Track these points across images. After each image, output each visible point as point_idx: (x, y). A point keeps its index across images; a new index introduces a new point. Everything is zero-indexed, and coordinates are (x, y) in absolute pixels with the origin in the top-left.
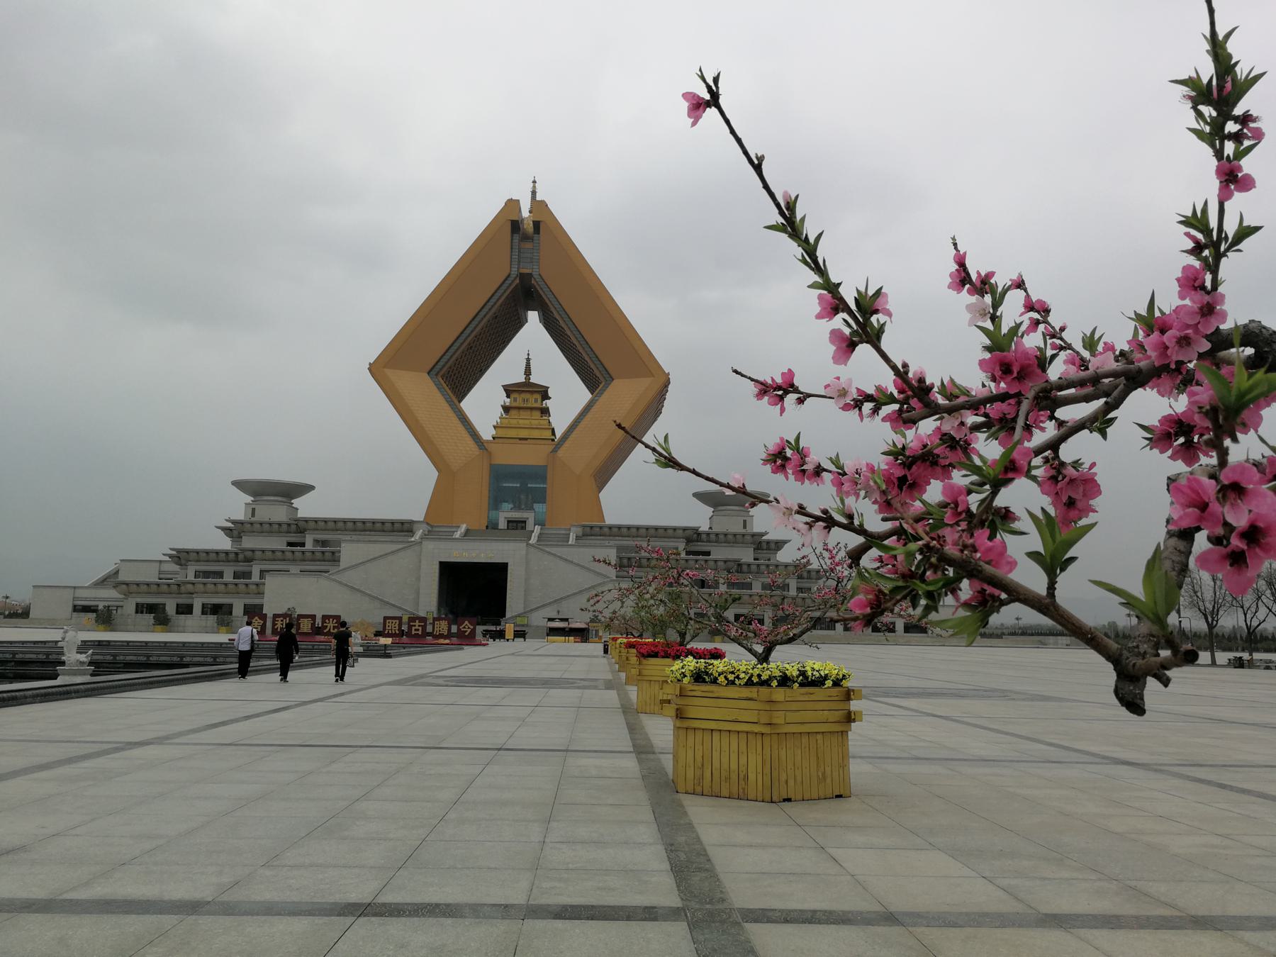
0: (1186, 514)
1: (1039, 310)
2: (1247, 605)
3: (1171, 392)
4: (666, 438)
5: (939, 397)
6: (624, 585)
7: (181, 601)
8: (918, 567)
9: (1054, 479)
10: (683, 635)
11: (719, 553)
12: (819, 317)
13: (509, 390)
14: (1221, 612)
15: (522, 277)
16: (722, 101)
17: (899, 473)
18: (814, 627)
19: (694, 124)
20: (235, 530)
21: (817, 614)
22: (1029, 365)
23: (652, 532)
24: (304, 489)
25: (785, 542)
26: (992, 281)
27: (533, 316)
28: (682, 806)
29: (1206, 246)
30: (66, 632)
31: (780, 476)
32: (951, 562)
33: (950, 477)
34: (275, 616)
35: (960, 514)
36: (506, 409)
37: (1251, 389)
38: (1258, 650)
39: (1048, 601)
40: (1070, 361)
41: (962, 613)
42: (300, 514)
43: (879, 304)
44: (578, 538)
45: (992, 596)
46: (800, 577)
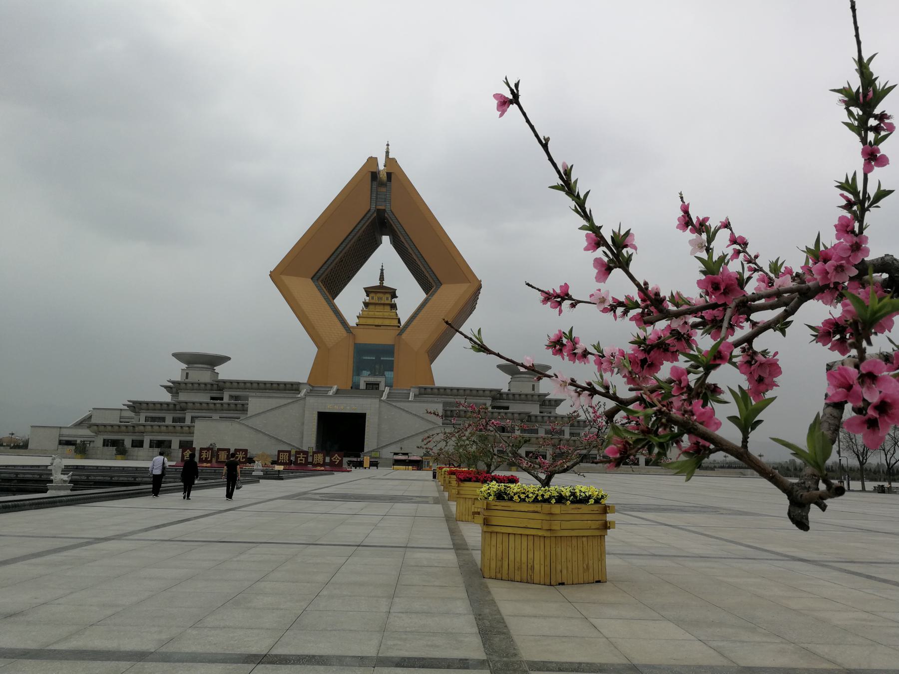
0: (837, 393)
1: (740, 243)
2: (887, 448)
3: (832, 301)
4: (479, 331)
5: (670, 304)
6: (448, 430)
7: (135, 438)
8: (653, 425)
9: (749, 363)
10: (489, 466)
11: (515, 408)
12: (586, 249)
13: (368, 291)
14: (869, 454)
15: (378, 210)
16: (520, 100)
17: (641, 356)
18: (581, 461)
19: (501, 115)
20: (174, 388)
21: (584, 452)
22: (732, 285)
23: (468, 392)
24: (223, 359)
25: (561, 401)
26: (707, 224)
27: (386, 239)
28: (487, 587)
29: (855, 204)
30: (54, 459)
31: (558, 357)
32: (676, 422)
33: (677, 360)
34: (202, 449)
35: (683, 388)
36: (366, 304)
37: (880, 309)
38: (895, 481)
39: (742, 450)
40: (761, 280)
41: (683, 458)
42: (220, 377)
43: (628, 241)
44: (415, 396)
45: (704, 446)
46: (572, 425)
